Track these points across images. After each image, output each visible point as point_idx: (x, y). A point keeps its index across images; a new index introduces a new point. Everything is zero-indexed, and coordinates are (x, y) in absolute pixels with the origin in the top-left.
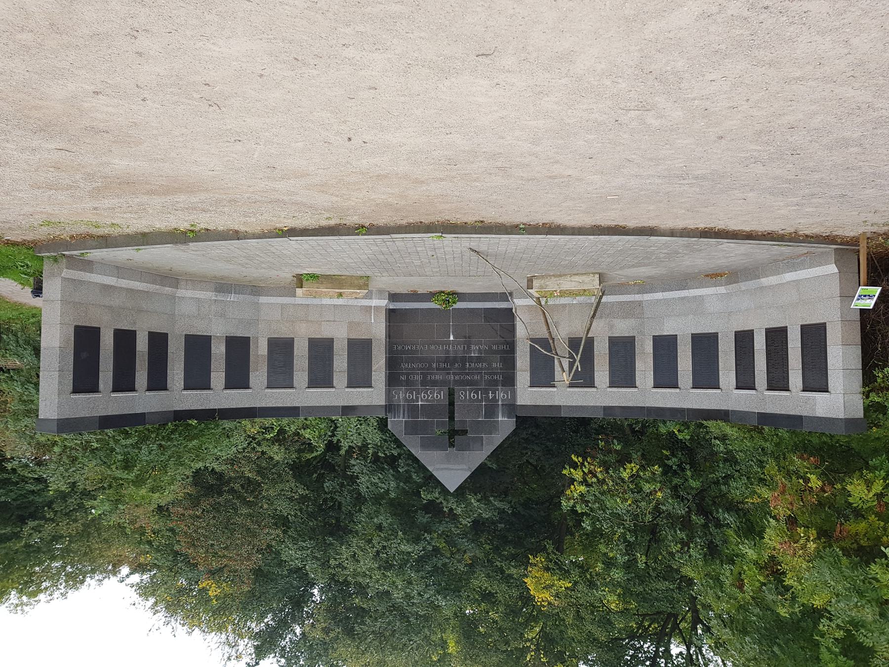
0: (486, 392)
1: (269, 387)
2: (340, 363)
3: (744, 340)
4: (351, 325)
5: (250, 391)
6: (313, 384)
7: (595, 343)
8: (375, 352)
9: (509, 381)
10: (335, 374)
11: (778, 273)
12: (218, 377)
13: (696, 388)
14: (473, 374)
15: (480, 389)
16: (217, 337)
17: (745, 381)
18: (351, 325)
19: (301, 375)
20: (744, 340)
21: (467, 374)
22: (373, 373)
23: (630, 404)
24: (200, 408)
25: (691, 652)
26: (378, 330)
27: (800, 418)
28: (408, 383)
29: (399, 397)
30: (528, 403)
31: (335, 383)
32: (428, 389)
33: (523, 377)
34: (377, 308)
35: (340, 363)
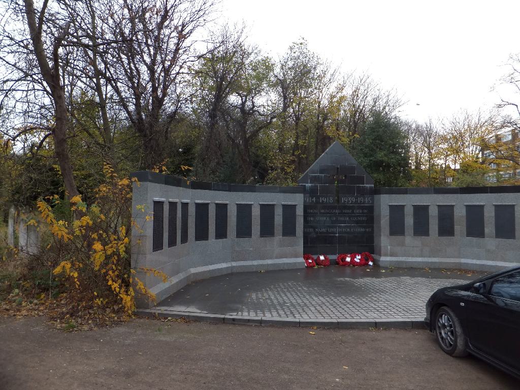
0: (317, 202)
1: (453, 206)
2: (409, 221)
3: (221, 233)
4: (402, 244)
5: (466, 204)
6: (426, 208)
7: (259, 233)
8: (281, 228)
9: (306, 208)
10: (412, 214)
11: (423, 262)
12: (256, 212)
13: (175, 203)
14: (324, 213)
15: (358, 204)
16: (491, 237)
17: (222, 209)
18: (402, 244)
19: (489, 215)
20: (221, 233)
21: (328, 213)
22: (388, 214)
23: (240, 193)
24: (502, 194)
25: (113, 44)
26: (385, 241)
27: (166, 184)
28: (363, 208)
29: (368, 199)
30: (297, 195)
31: (412, 209)
32: (351, 204)
33: (300, 211)
34: (386, 255)
35: (409, 221)
